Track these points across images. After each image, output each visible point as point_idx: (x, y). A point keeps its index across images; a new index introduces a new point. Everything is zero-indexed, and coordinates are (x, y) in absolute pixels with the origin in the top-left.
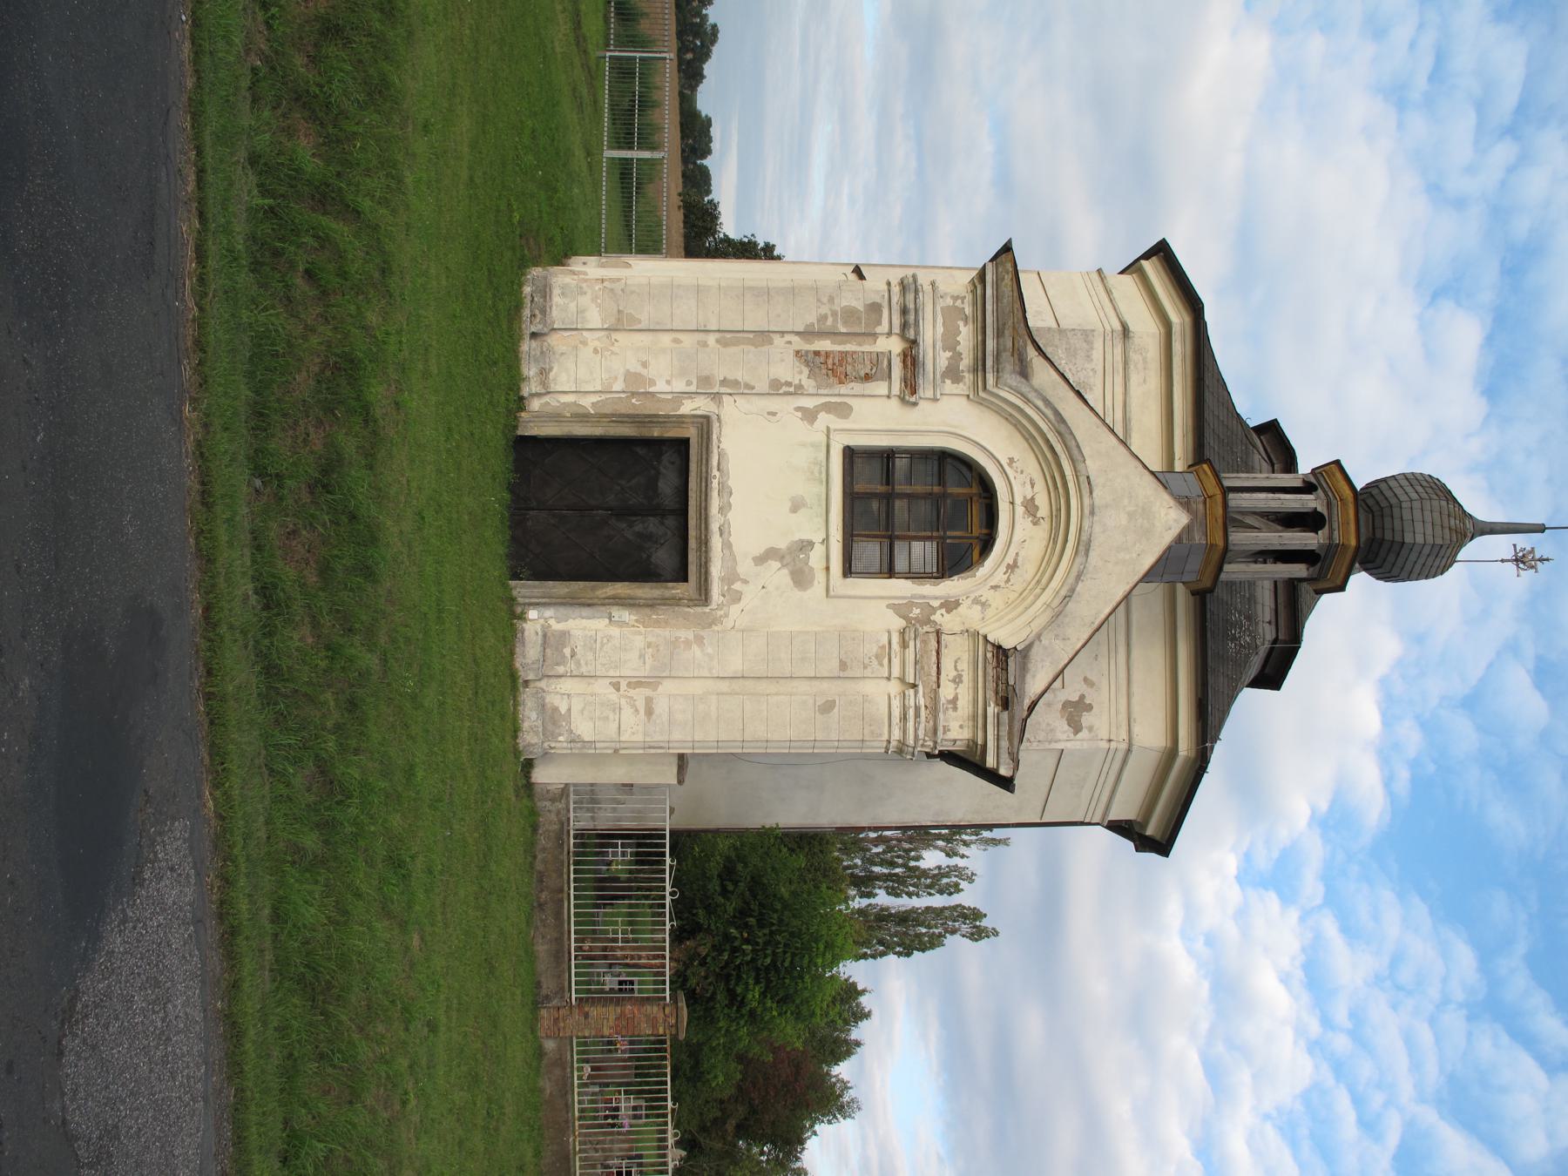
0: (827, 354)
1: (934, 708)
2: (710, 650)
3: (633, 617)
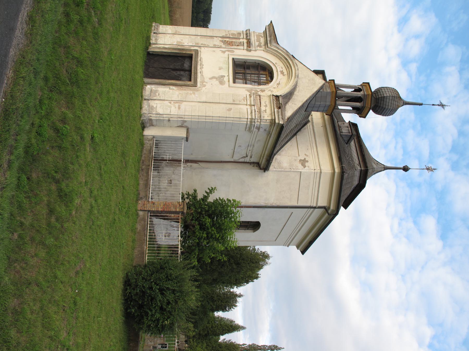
0: (228, 41)
1: (260, 112)
2: (197, 96)
3: (176, 88)
